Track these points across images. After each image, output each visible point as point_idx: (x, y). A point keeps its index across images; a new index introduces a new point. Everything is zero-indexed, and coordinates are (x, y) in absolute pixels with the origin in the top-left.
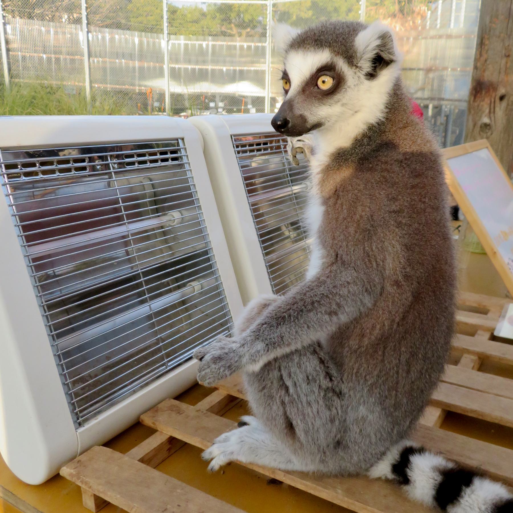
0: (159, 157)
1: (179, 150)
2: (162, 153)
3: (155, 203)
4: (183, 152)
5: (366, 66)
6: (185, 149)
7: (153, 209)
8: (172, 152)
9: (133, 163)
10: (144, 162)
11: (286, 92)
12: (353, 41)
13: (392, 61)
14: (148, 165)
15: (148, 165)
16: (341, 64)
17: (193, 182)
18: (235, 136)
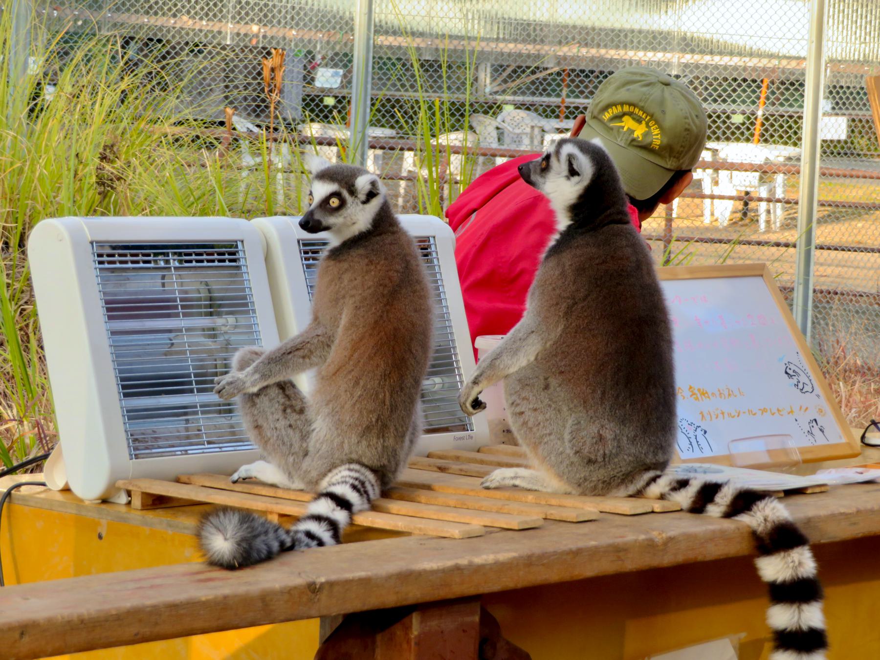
0: (216, 256)
1: (237, 252)
2: (219, 254)
3: (211, 306)
4: (241, 254)
5: (363, 197)
6: (244, 252)
7: (207, 304)
8: (230, 254)
9: (190, 261)
10: (202, 261)
11: (310, 205)
12: (356, 178)
13: (378, 194)
14: (205, 264)
15: (205, 264)
16: (345, 194)
17: (250, 284)
18: (302, 240)
